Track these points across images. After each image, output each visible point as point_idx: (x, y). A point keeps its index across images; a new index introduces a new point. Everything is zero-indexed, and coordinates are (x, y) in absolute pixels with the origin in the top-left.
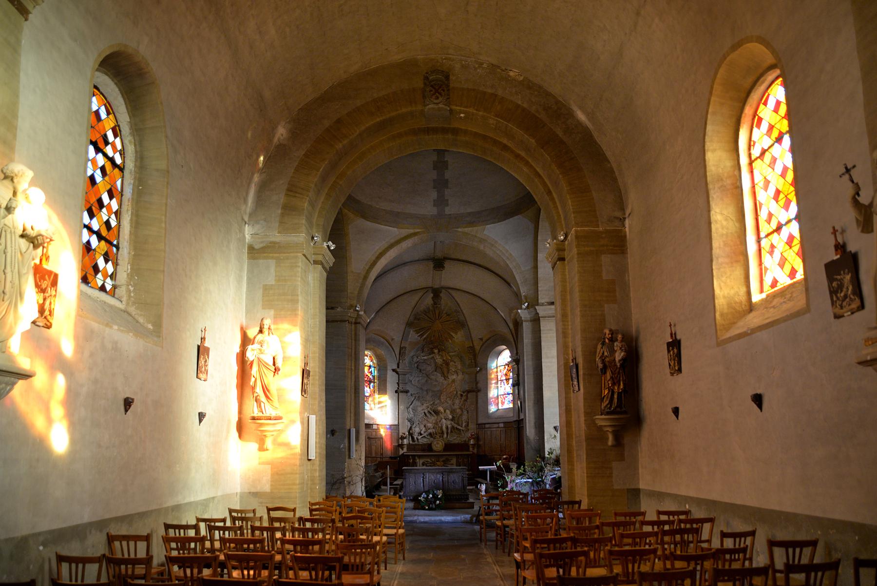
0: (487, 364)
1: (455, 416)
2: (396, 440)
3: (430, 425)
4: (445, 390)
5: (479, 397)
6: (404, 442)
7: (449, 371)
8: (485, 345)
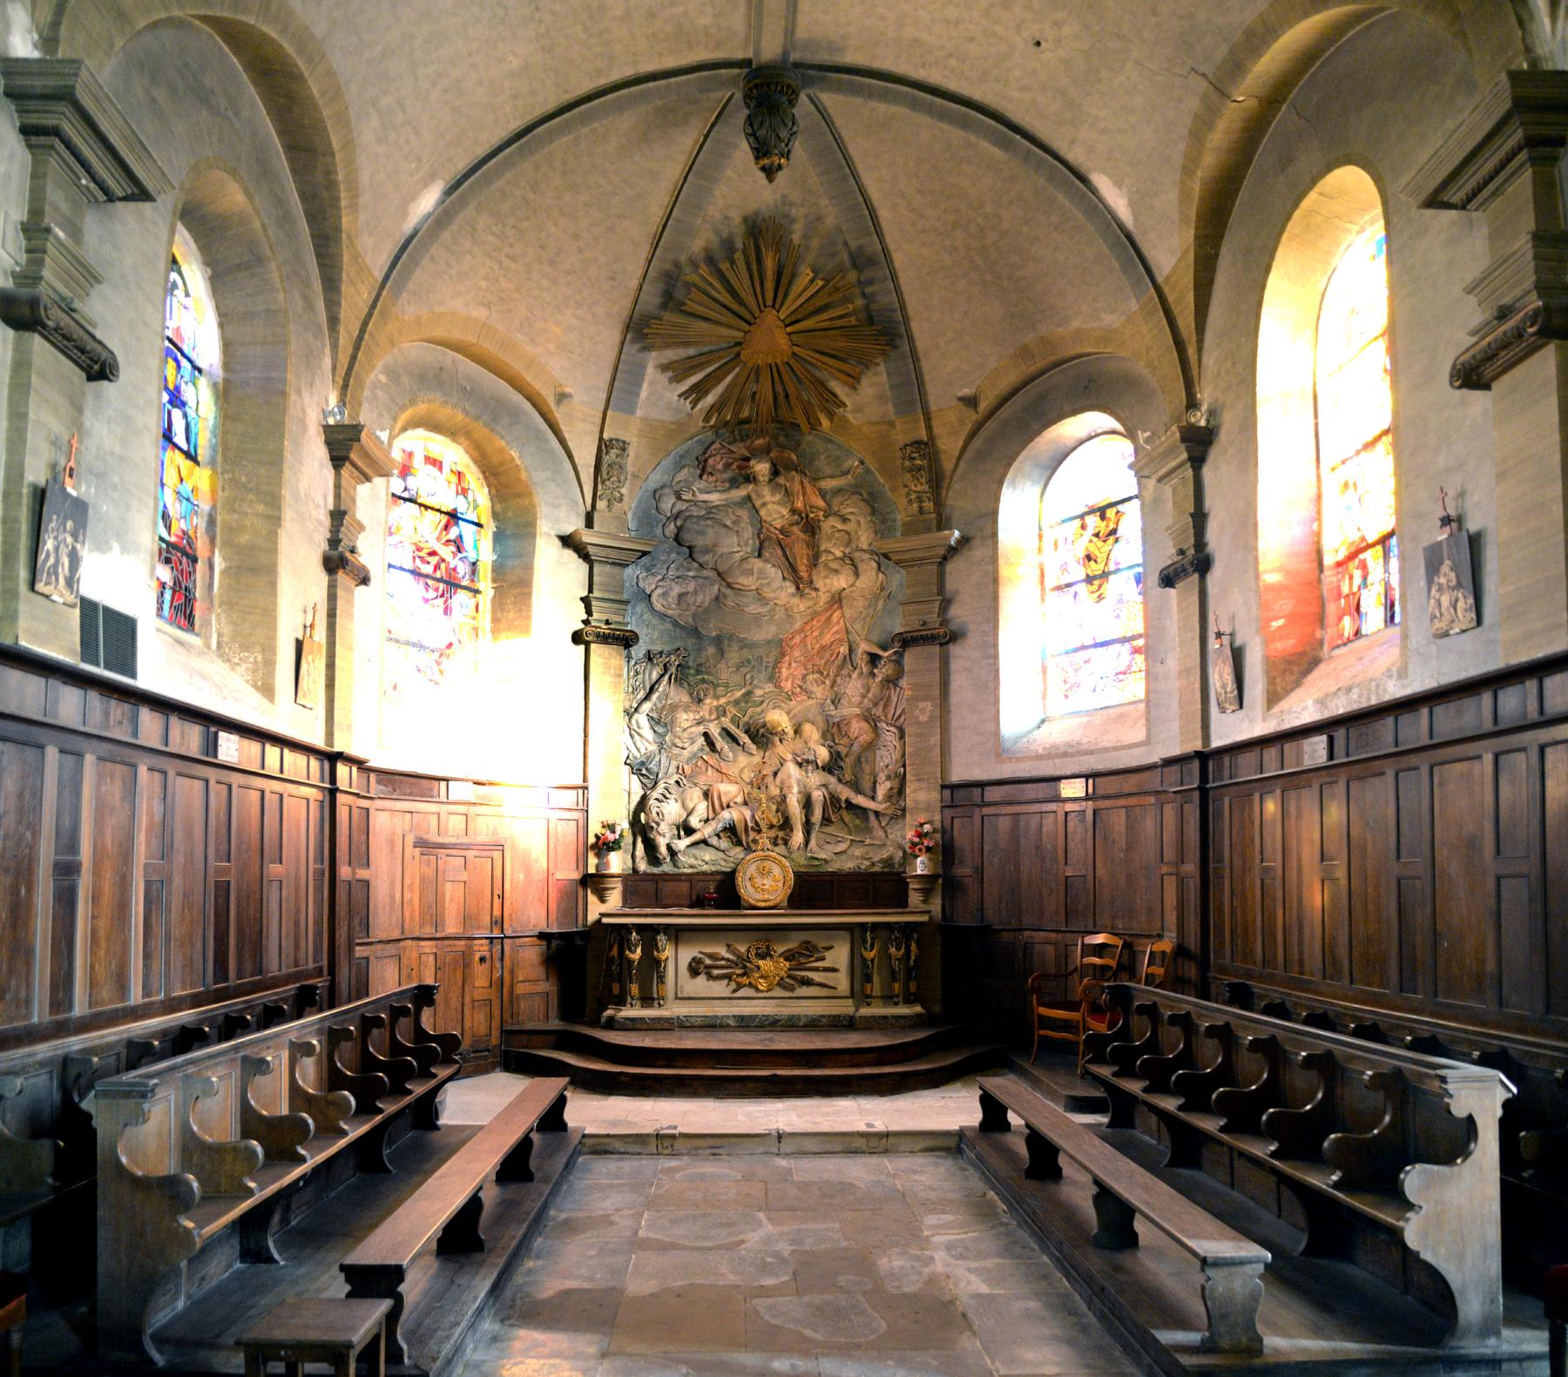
0: (993, 515)
1: (843, 750)
3: (728, 790)
4: (797, 639)
5: (955, 665)
6: (607, 865)
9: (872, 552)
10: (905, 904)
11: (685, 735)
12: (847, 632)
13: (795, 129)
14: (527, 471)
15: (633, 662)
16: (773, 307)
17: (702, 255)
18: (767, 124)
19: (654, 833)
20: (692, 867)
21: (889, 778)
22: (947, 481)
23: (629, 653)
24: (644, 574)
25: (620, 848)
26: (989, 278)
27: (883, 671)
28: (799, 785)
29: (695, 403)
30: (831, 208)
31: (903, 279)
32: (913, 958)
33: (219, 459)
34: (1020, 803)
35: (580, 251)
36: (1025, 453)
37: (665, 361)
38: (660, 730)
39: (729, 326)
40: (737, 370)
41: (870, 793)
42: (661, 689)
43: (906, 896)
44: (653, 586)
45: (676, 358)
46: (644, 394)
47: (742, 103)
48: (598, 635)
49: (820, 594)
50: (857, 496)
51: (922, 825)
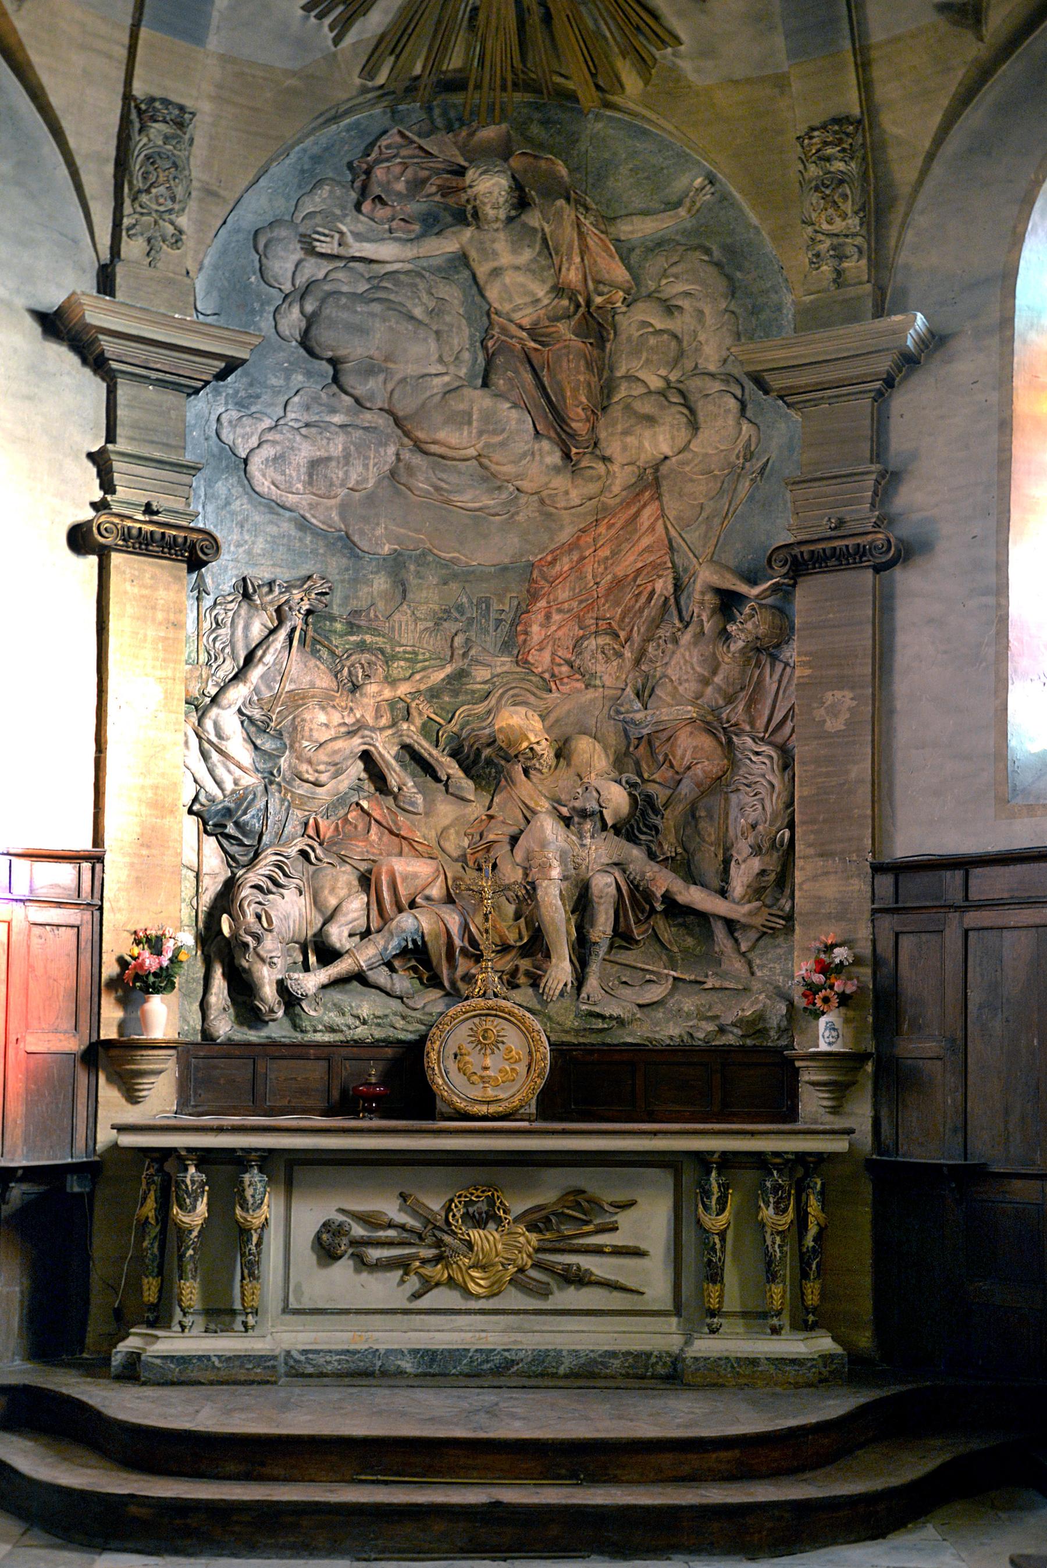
0: (1008, 276)
1: (660, 794)
2: (64, 1004)
4: (565, 564)
5: (905, 614)
6: (143, 1023)
7: (608, 389)
9: (729, 378)
10: (791, 1114)
11: (322, 756)
12: (671, 548)
15: (208, 601)
19: (250, 956)
20: (332, 1029)
21: (757, 850)
22: (901, 208)
23: (201, 577)
24: (234, 414)
28: (563, 861)
32: (813, 1230)
33: (436, 230)
41: (716, 883)
42: (269, 658)
43: (794, 1096)
44: (254, 441)
48: (126, 535)
49: (615, 468)
50: (698, 255)
51: (829, 948)
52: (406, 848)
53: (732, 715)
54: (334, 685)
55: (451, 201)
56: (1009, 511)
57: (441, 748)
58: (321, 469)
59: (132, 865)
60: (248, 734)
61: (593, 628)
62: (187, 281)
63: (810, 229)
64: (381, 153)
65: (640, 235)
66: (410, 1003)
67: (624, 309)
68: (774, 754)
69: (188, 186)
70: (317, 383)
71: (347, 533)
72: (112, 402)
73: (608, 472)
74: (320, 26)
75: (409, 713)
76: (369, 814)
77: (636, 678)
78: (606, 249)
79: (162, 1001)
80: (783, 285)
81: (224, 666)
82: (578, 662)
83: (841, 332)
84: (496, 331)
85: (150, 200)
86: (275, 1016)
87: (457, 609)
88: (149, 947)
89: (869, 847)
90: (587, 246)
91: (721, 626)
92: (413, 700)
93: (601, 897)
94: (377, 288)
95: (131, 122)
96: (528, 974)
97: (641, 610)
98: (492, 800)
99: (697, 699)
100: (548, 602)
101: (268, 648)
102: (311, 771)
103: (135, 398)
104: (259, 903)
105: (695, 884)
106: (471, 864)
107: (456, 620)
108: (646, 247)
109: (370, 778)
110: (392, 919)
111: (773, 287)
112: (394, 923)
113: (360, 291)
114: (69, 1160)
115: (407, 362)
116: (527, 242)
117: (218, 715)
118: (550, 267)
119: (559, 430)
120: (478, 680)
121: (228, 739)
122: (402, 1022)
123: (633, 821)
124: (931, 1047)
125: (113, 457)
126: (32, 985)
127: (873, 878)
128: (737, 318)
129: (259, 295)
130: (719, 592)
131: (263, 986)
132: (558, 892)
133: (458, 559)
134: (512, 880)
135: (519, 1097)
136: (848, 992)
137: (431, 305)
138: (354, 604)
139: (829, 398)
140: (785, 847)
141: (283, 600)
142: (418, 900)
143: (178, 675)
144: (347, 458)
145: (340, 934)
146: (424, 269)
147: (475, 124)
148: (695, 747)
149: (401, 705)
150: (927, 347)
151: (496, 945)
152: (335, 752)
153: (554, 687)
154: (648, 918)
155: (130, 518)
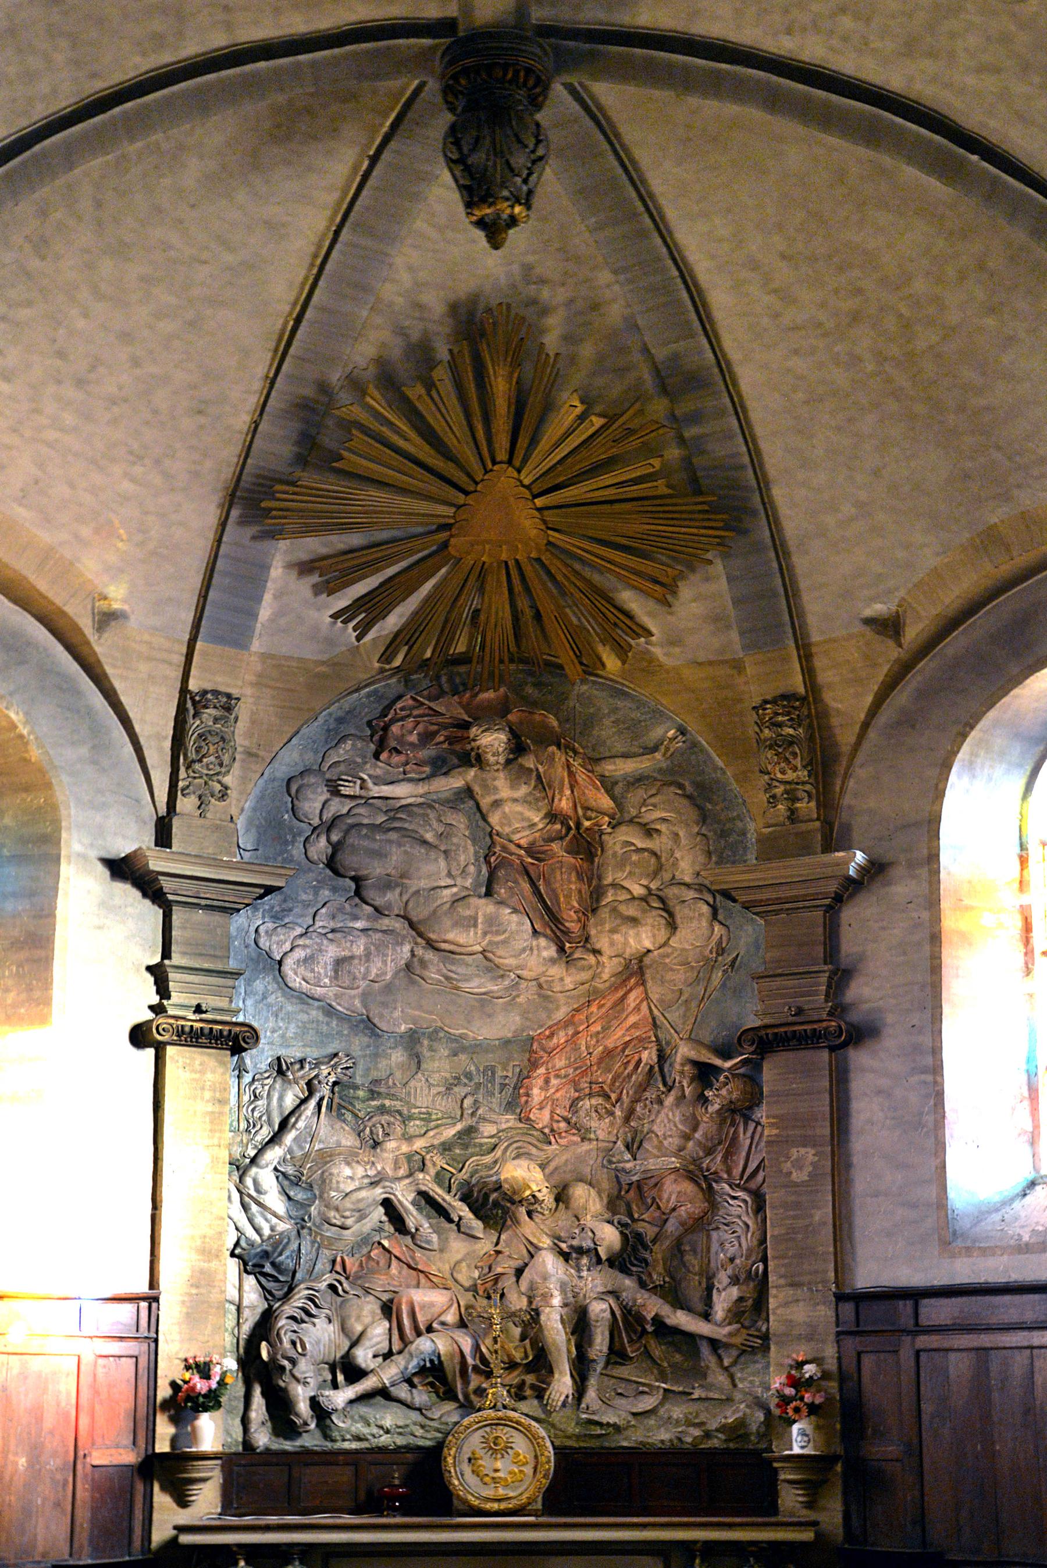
0: (933, 823)
1: (649, 1231)
2: (125, 1424)
4: (561, 1037)
5: (859, 1085)
6: (194, 1437)
7: (597, 894)
8: (914, 681)
9: (701, 888)
10: (772, 1509)
11: (348, 1204)
12: (655, 1025)
13: (540, 152)
14: (41, 746)
15: (247, 1078)
16: (510, 462)
17: (372, 370)
18: (487, 142)
19: (287, 1377)
20: (358, 1438)
21: (735, 1280)
22: (844, 762)
23: (241, 1060)
24: (270, 925)
25: (218, 1405)
26: (920, 408)
27: (718, 1097)
29: (363, 630)
30: (616, 288)
31: (756, 414)
33: (444, 770)
34: (989, 1329)
35: (136, 362)
36: (992, 714)
37: (304, 556)
38: (299, 1195)
39: (428, 498)
40: (443, 570)
41: (700, 1307)
42: (301, 1124)
43: (774, 1495)
44: (287, 946)
45: (324, 551)
46: (265, 612)
47: (439, 99)
48: (180, 1032)
49: (604, 959)
51: (800, 1365)
52: (423, 1280)
53: (712, 1164)
54: (358, 1144)
55: (457, 747)
56: (941, 1007)
57: (452, 1194)
58: (346, 966)
59: (183, 1302)
60: (282, 1187)
61: (587, 1091)
62: (232, 825)
63: (766, 777)
64: (396, 714)
65: (622, 772)
66: (429, 1414)
67: (609, 830)
68: (748, 1199)
69: (233, 753)
70: (341, 896)
71: (368, 1017)
72: (167, 925)
73: (598, 962)
74: (346, 629)
75: (424, 1164)
76: (389, 1252)
77: (626, 1133)
78: (594, 784)
79: (211, 1418)
80: (747, 815)
81: (262, 1132)
82: (574, 1119)
83: (793, 863)
84: (497, 849)
85: (202, 767)
86: (308, 1428)
87: (466, 1077)
88: (198, 1372)
89: (833, 1279)
90: (576, 781)
91: (700, 1091)
92: (427, 1153)
93: (597, 1321)
94: (394, 819)
95: (187, 710)
96: (533, 1387)
97: (630, 1076)
98: (499, 1238)
99: (680, 1151)
100: (547, 1069)
101: (300, 1116)
102: (338, 1216)
103: (187, 921)
104: (294, 1331)
105: (682, 1309)
106: (481, 1292)
107: (465, 1085)
108: (628, 782)
109: (390, 1221)
110: (412, 1342)
111: (738, 815)
112: (414, 1345)
113: (378, 822)
114: (127, 1558)
115: (419, 879)
116: (523, 780)
117: (256, 1174)
118: (544, 799)
119: (554, 928)
120: (486, 1134)
121: (265, 1193)
122: (421, 1431)
123: (625, 1256)
124: (892, 1450)
125: (168, 970)
126: (97, 1407)
127: (837, 1305)
128: (708, 839)
129: (291, 829)
130: (696, 1064)
131: (298, 1402)
132: (559, 1317)
133: (466, 1034)
134: (518, 1307)
135: (526, 1495)
136: (817, 1402)
137: (441, 830)
138: (375, 1075)
139: (788, 909)
140: (760, 1277)
141: (313, 1075)
142: (435, 1325)
143: (222, 1142)
144: (368, 956)
145: (365, 1356)
146: (434, 801)
147: (477, 689)
148: (679, 1193)
149: (417, 1157)
150: (869, 872)
151: (504, 1363)
152: (359, 1201)
153: (553, 1140)
154: (640, 1338)
155: (184, 1018)
